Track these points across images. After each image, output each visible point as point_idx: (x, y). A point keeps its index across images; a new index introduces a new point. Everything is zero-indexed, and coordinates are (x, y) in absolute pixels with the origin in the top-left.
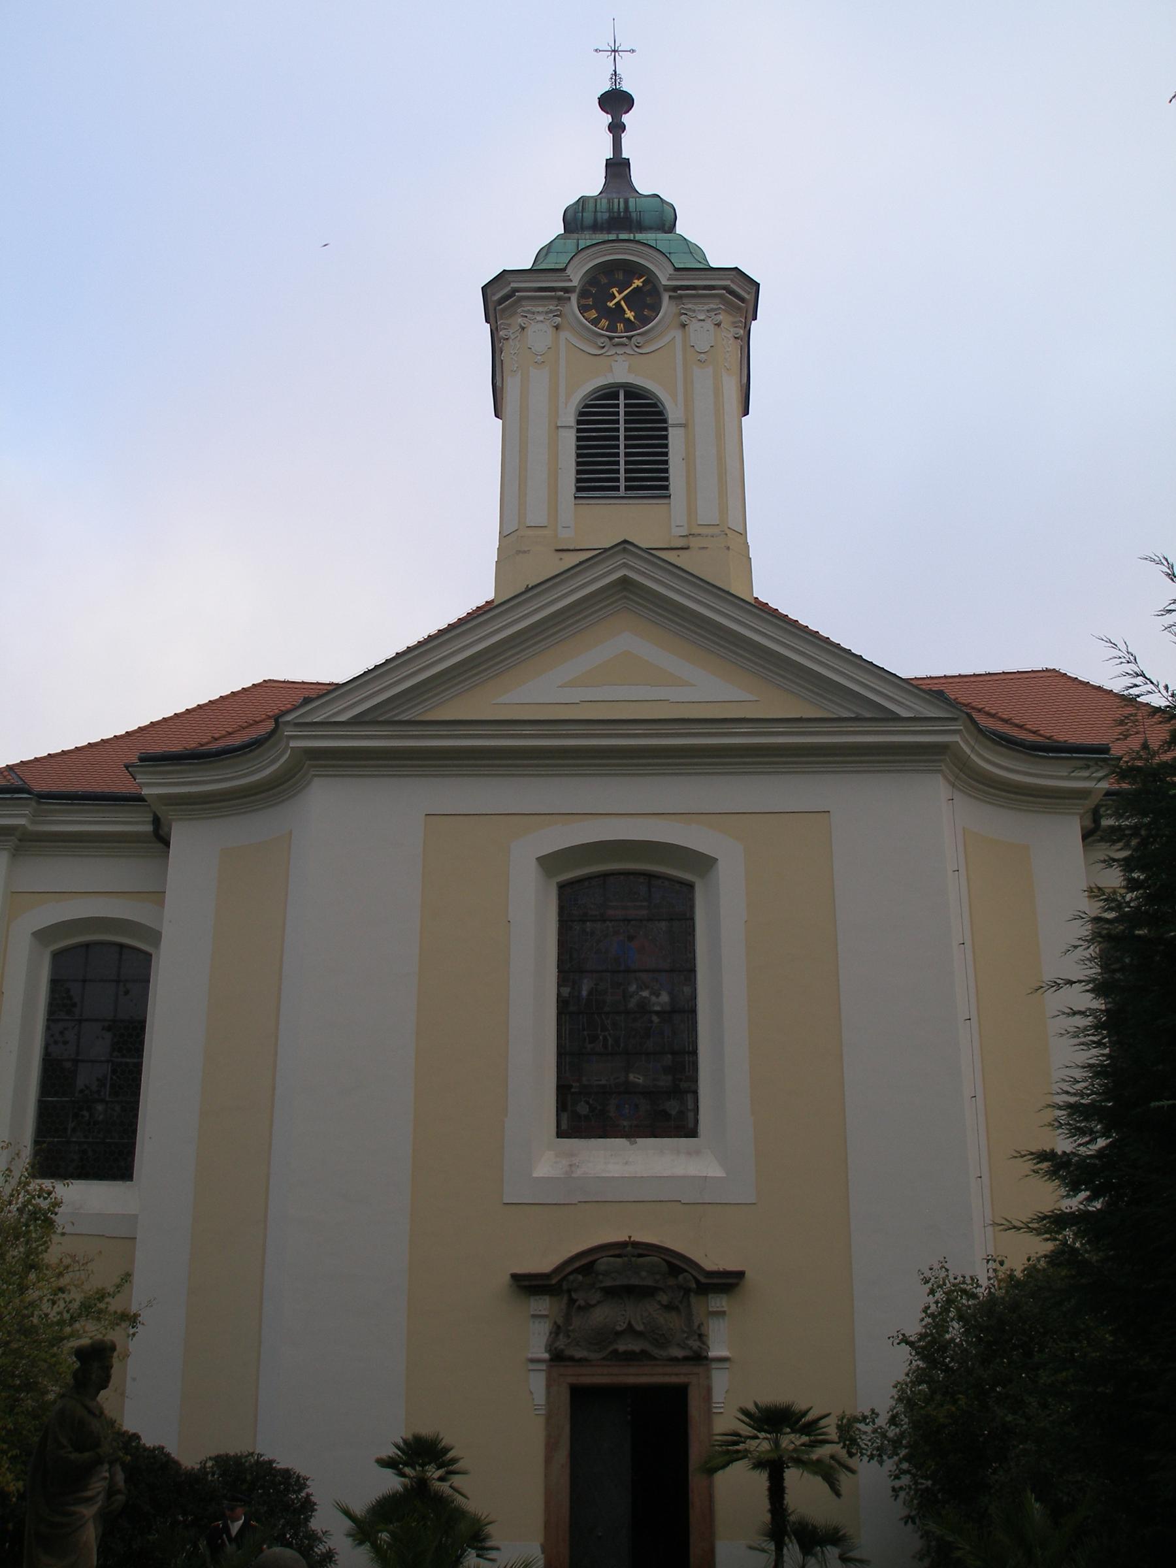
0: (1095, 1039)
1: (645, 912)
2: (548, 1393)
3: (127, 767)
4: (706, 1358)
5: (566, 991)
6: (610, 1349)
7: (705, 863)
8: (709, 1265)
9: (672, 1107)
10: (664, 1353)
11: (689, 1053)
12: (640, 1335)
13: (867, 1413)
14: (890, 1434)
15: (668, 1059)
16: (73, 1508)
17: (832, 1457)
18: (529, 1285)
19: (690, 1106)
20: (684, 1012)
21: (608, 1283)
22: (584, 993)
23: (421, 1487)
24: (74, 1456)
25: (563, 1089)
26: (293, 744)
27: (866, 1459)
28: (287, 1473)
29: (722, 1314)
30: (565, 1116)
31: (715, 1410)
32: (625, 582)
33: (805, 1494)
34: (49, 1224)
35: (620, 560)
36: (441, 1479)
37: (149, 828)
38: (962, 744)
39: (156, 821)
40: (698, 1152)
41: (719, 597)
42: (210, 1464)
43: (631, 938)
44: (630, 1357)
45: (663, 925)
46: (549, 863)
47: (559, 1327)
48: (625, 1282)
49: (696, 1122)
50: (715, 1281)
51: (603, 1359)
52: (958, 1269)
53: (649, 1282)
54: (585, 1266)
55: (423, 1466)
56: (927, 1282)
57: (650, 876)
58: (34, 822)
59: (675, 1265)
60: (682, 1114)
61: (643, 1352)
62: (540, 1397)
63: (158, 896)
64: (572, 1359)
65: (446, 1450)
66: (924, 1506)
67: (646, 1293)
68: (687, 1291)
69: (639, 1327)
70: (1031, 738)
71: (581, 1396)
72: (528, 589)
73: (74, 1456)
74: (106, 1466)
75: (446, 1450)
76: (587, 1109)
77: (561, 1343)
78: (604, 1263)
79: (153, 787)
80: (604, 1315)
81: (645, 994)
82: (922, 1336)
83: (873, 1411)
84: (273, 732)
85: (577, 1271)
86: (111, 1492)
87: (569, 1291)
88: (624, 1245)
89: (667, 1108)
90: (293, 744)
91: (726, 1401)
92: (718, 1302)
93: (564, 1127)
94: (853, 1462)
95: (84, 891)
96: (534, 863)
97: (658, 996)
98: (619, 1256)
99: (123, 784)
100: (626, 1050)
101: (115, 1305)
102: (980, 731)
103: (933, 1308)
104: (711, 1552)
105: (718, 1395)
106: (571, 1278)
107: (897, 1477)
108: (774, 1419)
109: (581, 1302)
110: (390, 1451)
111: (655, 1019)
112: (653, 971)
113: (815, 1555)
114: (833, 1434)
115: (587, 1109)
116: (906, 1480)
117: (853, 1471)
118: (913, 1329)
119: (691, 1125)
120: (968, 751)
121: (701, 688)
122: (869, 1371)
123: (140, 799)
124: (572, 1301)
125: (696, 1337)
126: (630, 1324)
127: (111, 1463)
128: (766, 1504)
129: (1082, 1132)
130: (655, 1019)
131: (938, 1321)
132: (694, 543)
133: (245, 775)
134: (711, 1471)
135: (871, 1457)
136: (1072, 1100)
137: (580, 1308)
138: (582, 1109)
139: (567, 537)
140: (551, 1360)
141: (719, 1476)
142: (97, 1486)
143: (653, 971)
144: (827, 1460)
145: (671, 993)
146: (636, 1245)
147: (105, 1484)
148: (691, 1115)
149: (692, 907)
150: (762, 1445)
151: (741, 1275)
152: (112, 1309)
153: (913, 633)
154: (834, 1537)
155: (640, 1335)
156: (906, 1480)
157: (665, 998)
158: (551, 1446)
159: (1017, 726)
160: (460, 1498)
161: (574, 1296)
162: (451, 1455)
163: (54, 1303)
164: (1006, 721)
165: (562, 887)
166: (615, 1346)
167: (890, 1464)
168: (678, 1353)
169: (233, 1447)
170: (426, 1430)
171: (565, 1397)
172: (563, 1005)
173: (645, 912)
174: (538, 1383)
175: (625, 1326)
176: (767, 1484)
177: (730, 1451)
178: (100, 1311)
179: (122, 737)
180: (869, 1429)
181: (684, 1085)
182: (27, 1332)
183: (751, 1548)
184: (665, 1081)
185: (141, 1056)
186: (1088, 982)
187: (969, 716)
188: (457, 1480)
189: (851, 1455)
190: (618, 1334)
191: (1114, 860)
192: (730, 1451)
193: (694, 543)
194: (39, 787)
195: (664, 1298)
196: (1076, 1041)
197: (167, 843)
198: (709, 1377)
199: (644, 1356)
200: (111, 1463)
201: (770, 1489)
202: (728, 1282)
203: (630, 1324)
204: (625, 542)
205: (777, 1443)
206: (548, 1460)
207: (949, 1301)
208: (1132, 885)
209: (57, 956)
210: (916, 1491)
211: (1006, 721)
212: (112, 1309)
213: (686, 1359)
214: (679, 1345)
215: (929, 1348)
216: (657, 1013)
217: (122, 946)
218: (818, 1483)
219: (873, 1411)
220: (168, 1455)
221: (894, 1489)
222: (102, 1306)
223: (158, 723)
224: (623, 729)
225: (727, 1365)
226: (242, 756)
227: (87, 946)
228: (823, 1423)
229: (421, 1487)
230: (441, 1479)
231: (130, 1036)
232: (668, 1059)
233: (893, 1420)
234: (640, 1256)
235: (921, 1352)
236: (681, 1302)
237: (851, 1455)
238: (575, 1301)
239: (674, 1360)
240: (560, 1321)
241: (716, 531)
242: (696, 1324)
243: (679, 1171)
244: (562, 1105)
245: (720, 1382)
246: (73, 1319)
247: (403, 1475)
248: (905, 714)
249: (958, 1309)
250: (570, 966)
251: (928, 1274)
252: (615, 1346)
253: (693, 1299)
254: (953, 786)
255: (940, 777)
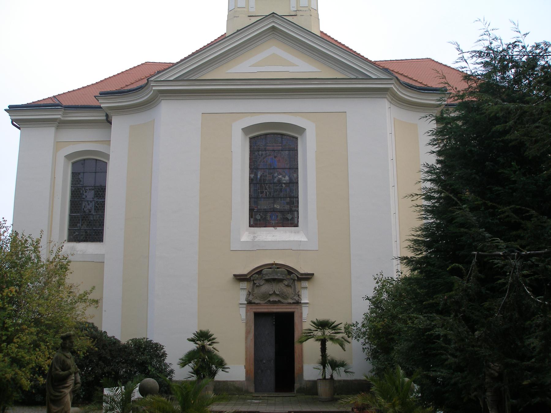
0: (424, 216)
1: (280, 148)
2: (246, 315)
3: (95, 97)
4: (300, 303)
5: (252, 176)
7: (301, 130)
8: (302, 271)
9: (289, 216)
10: (286, 301)
11: (296, 197)
13: (355, 323)
14: (362, 330)
15: (288, 200)
16: (62, 390)
17: (342, 338)
18: (240, 278)
19: (296, 216)
20: (294, 183)
21: (267, 278)
22: (259, 177)
23: (202, 349)
24: (62, 373)
25: (251, 210)
26: (154, 88)
27: (354, 338)
28: (156, 344)
30: (252, 220)
32: (273, 27)
33: (333, 350)
34: (66, 269)
35: (271, 20)
36: (210, 345)
37: (105, 118)
38: (394, 88)
39: (107, 116)
40: (298, 232)
41: (308, 34)
42: (130, 342)
43: (275, 157)
44: (274, 302)
45: (287, 152)
46: (246, 130)
48: (273, 277)
49: (298, 221)
52: (386, 275)
54: (259, 271)
55: (203, 341)
56: (376, 279)
57: (282, 135)
58: (63, 117)
59: (290, 271)
60: (293, 218)
62: (244, 317)
63: (108, 142)
64: (254, 303)
65: (211, 336)
66: (374, 355)
67: (280, 281)
68: (294, 280)
69: (278, 293)
70: (420, 85)
71: (257, 315)
72: (238, 31)
73: (62, 373)
74: (73, 375)
75: (211, 336)
76: (259, 217)
77: (251, 298)
78: (265, 271)
79: (105, 104)
80: (266, 288)
81: (280, 177)
82: (373, 298)
83: (357, 322)
84: (147, 84)
85: (257, 273)
86: (76, 383)
87: (253, 280)
88: (272, 264)
89: (288, 217)
90: (154, 88)
91: (306, 318)
92: (305, 284)
93: (252, 223)
94: (349, 339)
95: (82, 141)
96: (241, 130)
97: (285, 177)
98: (270, 268)
99: (95, 103)
100: (274, 194)
101: (91, 297)
102: (401, 83)
103: (378, 288)
104: (302, 368)
105: (304, 316)
106: (254, 276)
107: (364, 345)
108: (323, 325)
110: (192, 336)
111: (284, 185)
112: (283, 169)
113: (336, 370)
114: (343, 331)
115: (259, 217)
116: (367, 346)
117: (349, 343)
118: (371, 294)
119: (296, 222)
120: (396, 91)
121: (301, 67)
122: (356, 309)
123: (100, 107)
124: (254, 284)
127: (75, 373)
128: (320, 353)
129: (417, 250)
130: (284, 185)
131: (379, 292)
132: (298, 13)
133: (136, 100)
134: (301, 342)
135: (356, 338)
136: (415, 238)
137: (257, 286)
138: (258, 217)
139: (253, 11)
141: (305, 344)
142: (70, 382)
143: (283, 169)
144: (341, 339)
145: (289, 177)
146: (276, 264)
147: (73, 381)
148: (296, 219)
149: (297, 146)
150: (319, 333)
151: (313, 274)
152: (89, 298)
153: (377, 47)
154: (343, 365)
156: (367, 346)
157: (287, 178)
158: (247, 333)
159: (414, 80)
160: (216, 351)
161: (255, 282)
162: (213, 337)
163: (69, 297)
164: (411, 79)
165: (251, 139)
166: (269, 299)
167: (362, 340)
168: (291, 301)
169: (138, 337)
170: (204, 329)
172: (251, 181)
173: (280, 148)
174: (243, 312)
176: (320, 346)
177: (308, 335)
178: (85, 299)
179: (94, 84)
180: (355, 328)
181: (293, 209)
182: (60, 306)
184: (287, 207)
185: (105, 199)
186: (424, 195)
187: (397, 78)
188: (215, 345)
189: (349, 337)
190: (270, 295)
191: (434, 152)
192: (308, 335)
193: (298, 13)
194: (65, 103)
195: (286, 283)
196: (419, 214)
197: (111, 123)
198: (301, 310)
199: (279, 302)
200: (75, 373)
201: (321, 348)
202: (308, 277)
204: (273, 13)
205: (324, 333)
206: (246, 338)
207: (383, 286)
208: (439, 162)
209: (73, 164)
210: (371, 349)
211: (411, 79)
212: (89, 298)
213: (293, 303)
215: (376, 302)
216: (284, 183)
217: (96, 160)
218: (338, 346)
219: (357, 322)
220: (116, 339)
221: (363, 349)
222: (86, 297)
223: (107, 79)
224: (272, 82)
225: (308, 305)
226: (137, 92)
227: (84, 160)
228: (339, 326)
229: (202, 349)
230: (210, 345)
231: (100, 192)
232: (288, 200)
233: (363, 326)
234: (278, 268)
235: (374, 303)
237: (349, 337)
241: (306, 9)
243: (292, 239)
244: (251, 216)
245: (305, 311)
246: (76, 302)
247: (197, 344)
248: (374, 77)
249: (386, 289)
250: (253, 167)
251: (376, 276)
252: (269, 299)
253: (296, 283)
254: (391, 103)
255: (386, 100)
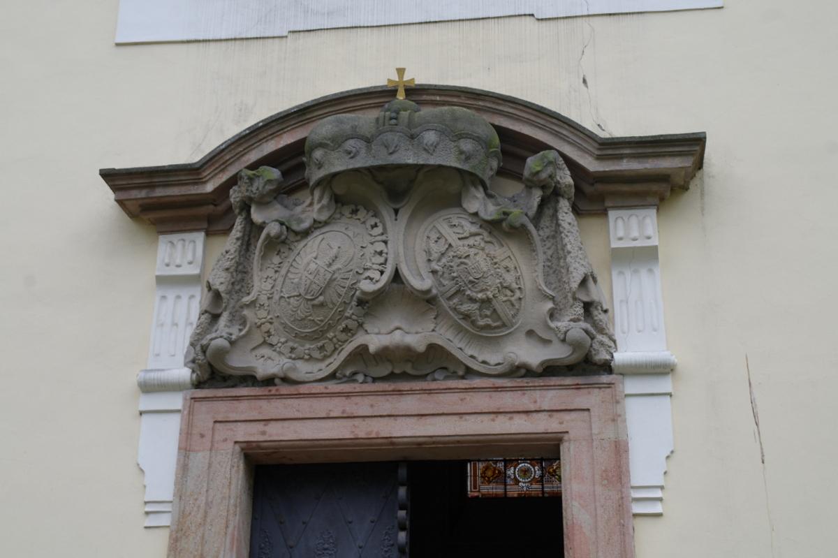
2: (183, 469)
4: (607, 367)
6: (349, 348)
10: (494, 357)
12: (426, 302)
29: (647, 256)
31: (637, 508)
47: (217, 296)
50: (627, 166)
51: (332, 376)
53: (449, 159)
61: (434, 349)
62: (162, 484)
64: (248, 379)
68: (552, 194)
69: (420, 281)
71: (278, 481)
88: (388, 93)
92: (631, 227)
109: (273, 229)
125: (580, 310)
126: (397, 277)
140: (198, 385)
151: (693, 144)
155: (426, 302)
161: (257, 216)
168: (533, 355)
171: (229, 482)
174: (157, 444)
175: (385, 279)
183: (567, 432)
198: (616, 419)
202: (660, 172)
203: (397, 277)
213: (550, 370)
214: (530, 333)
225: (664, 385)
236: (536, 219)
237: (575, 478)
238: (261, 227)
239: (520, 372)
240: (220, 281)
242: (577, 278)
252: (360, 339)
